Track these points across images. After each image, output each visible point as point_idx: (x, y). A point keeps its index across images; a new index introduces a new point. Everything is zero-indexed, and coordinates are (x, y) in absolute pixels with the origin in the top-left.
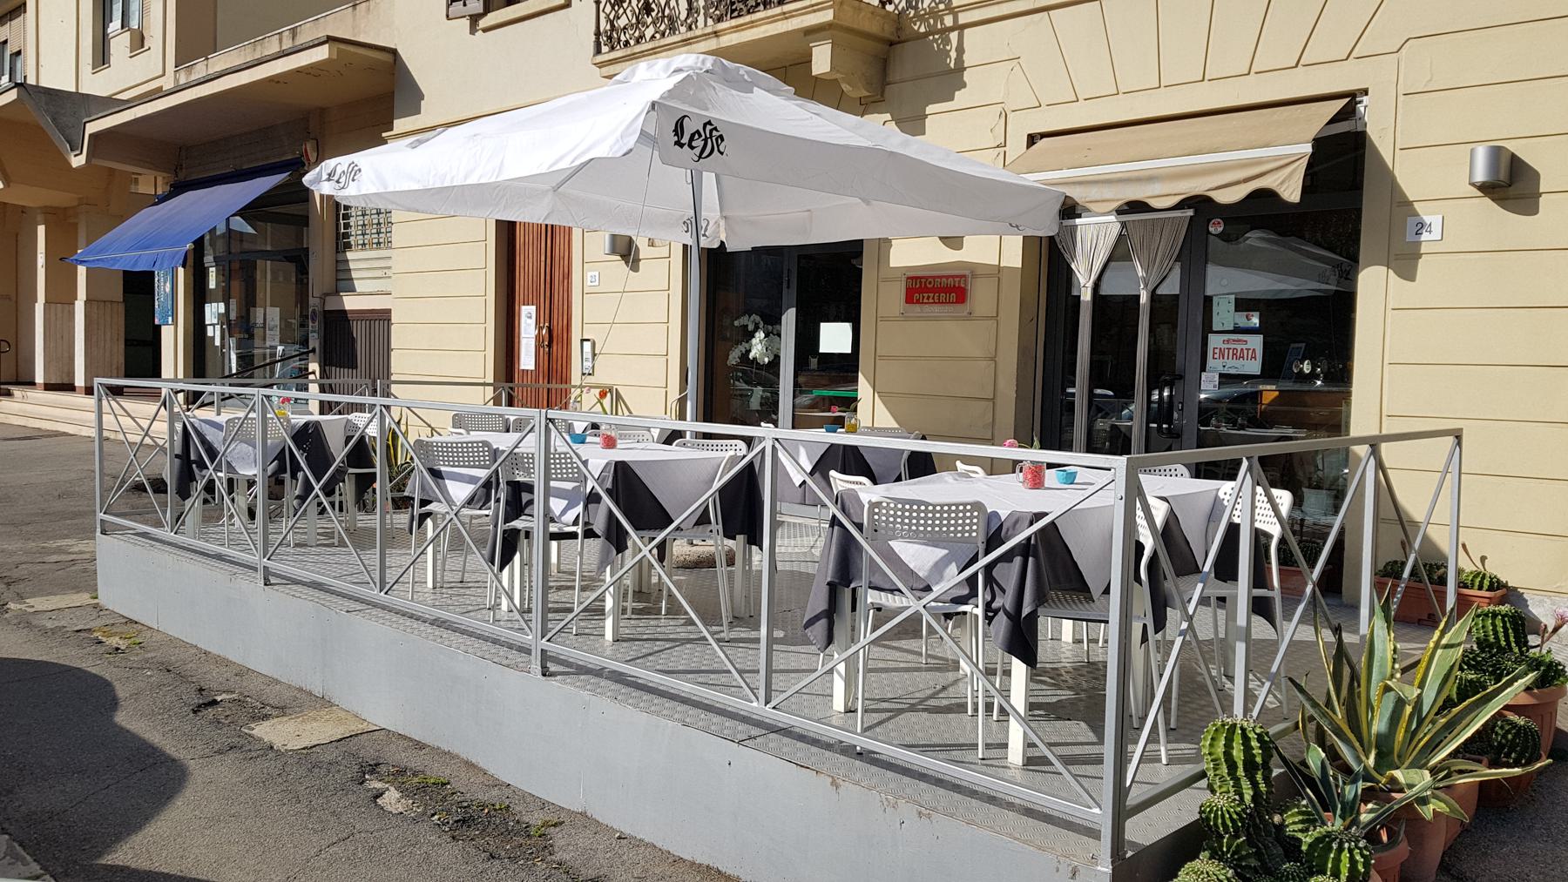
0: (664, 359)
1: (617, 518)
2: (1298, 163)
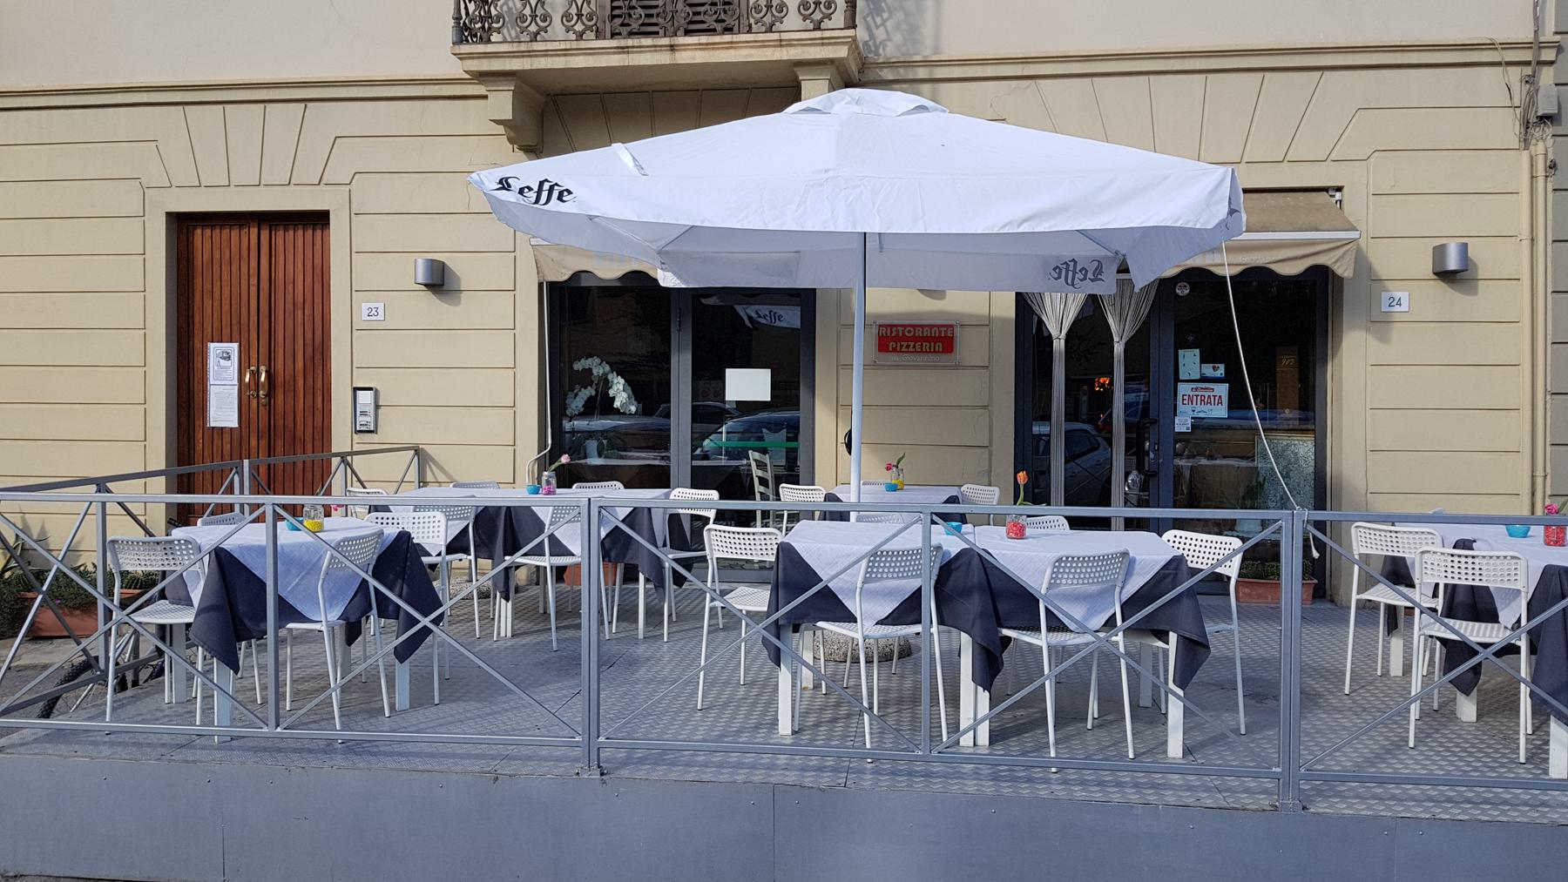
0: (511, 411)
1: (129, 605)
2: (1349, 246)
